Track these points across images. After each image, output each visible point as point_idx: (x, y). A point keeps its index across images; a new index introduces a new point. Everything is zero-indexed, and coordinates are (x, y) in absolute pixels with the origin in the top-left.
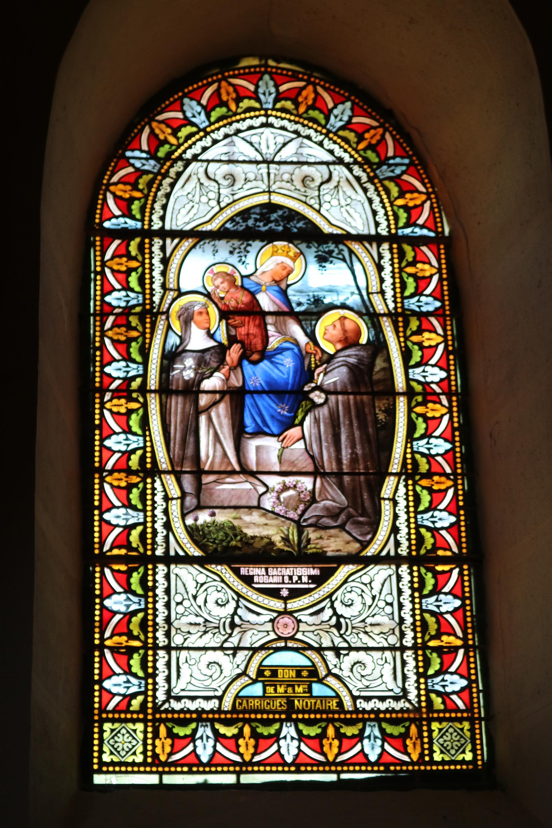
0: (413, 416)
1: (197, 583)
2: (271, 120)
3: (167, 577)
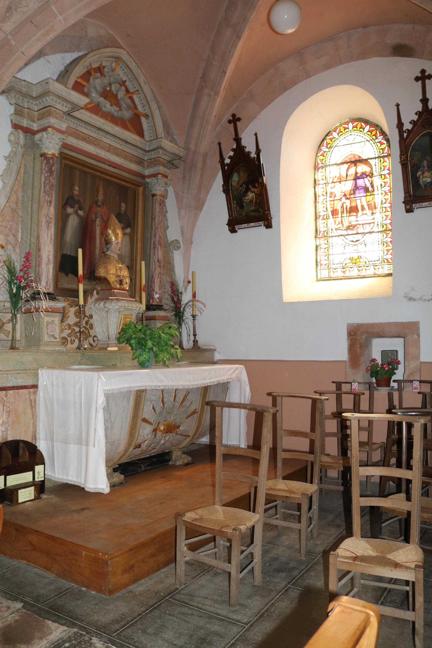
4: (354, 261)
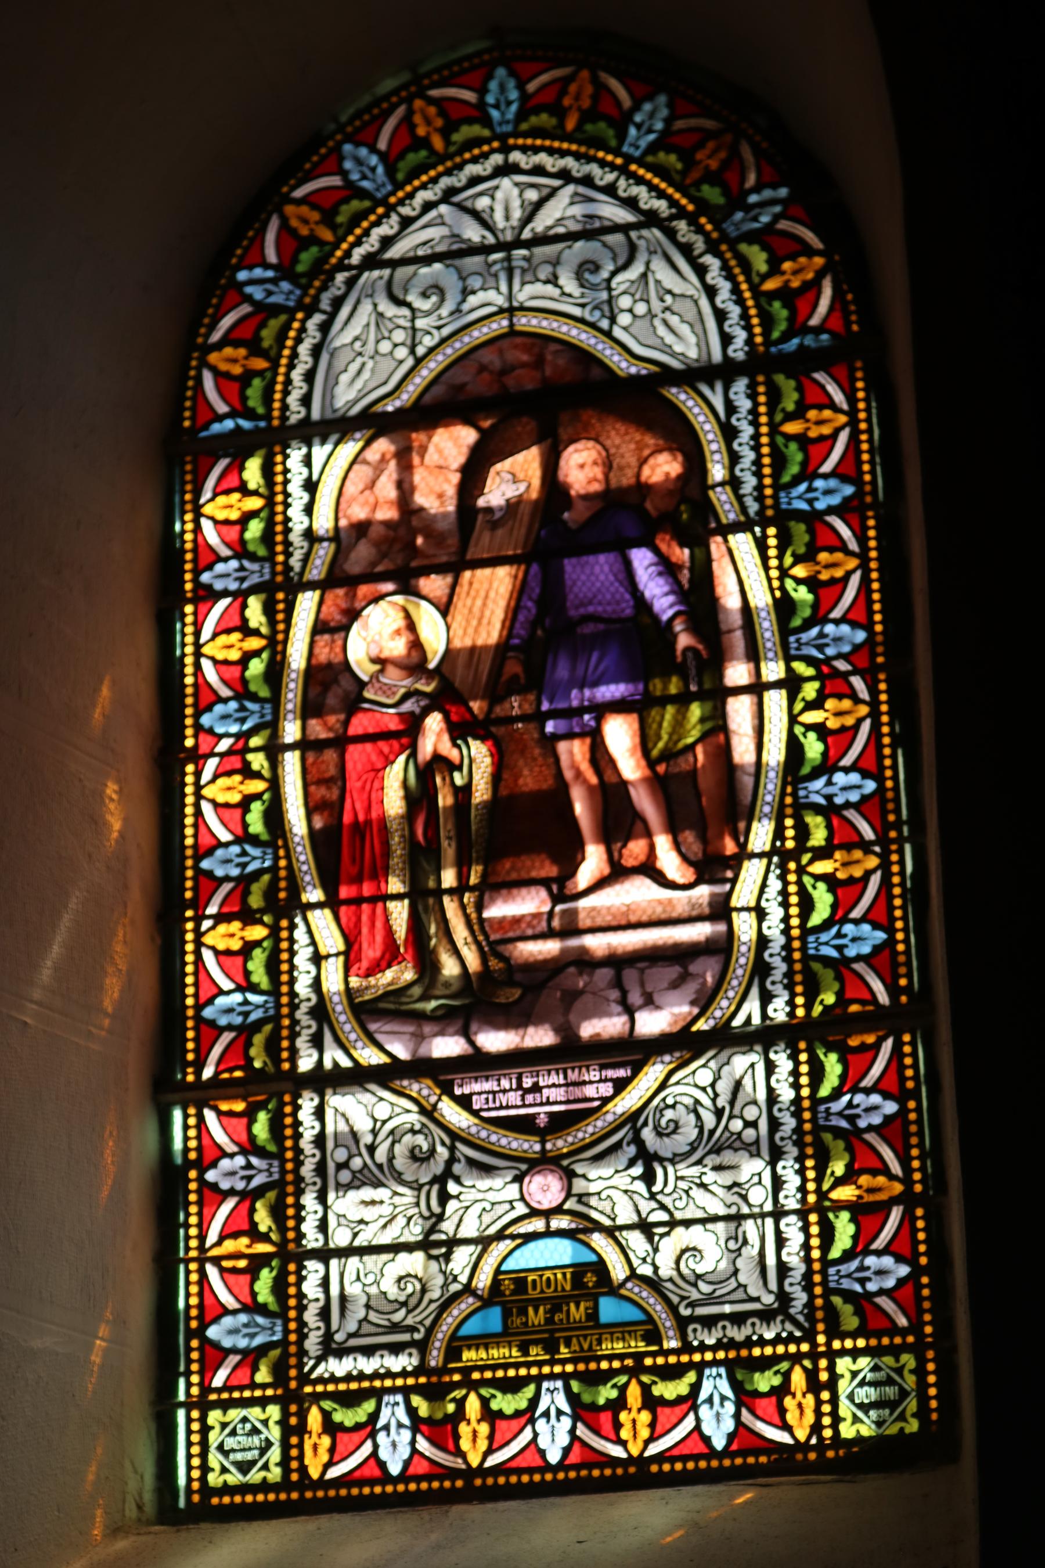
0: (798, 730)
1: (375, 1121)
2: (516, 156)
3: (320, 1113)
4: (536, 1317)
